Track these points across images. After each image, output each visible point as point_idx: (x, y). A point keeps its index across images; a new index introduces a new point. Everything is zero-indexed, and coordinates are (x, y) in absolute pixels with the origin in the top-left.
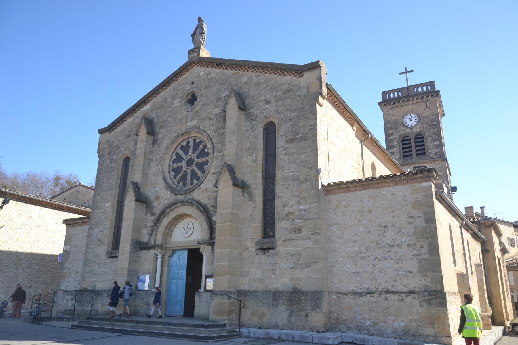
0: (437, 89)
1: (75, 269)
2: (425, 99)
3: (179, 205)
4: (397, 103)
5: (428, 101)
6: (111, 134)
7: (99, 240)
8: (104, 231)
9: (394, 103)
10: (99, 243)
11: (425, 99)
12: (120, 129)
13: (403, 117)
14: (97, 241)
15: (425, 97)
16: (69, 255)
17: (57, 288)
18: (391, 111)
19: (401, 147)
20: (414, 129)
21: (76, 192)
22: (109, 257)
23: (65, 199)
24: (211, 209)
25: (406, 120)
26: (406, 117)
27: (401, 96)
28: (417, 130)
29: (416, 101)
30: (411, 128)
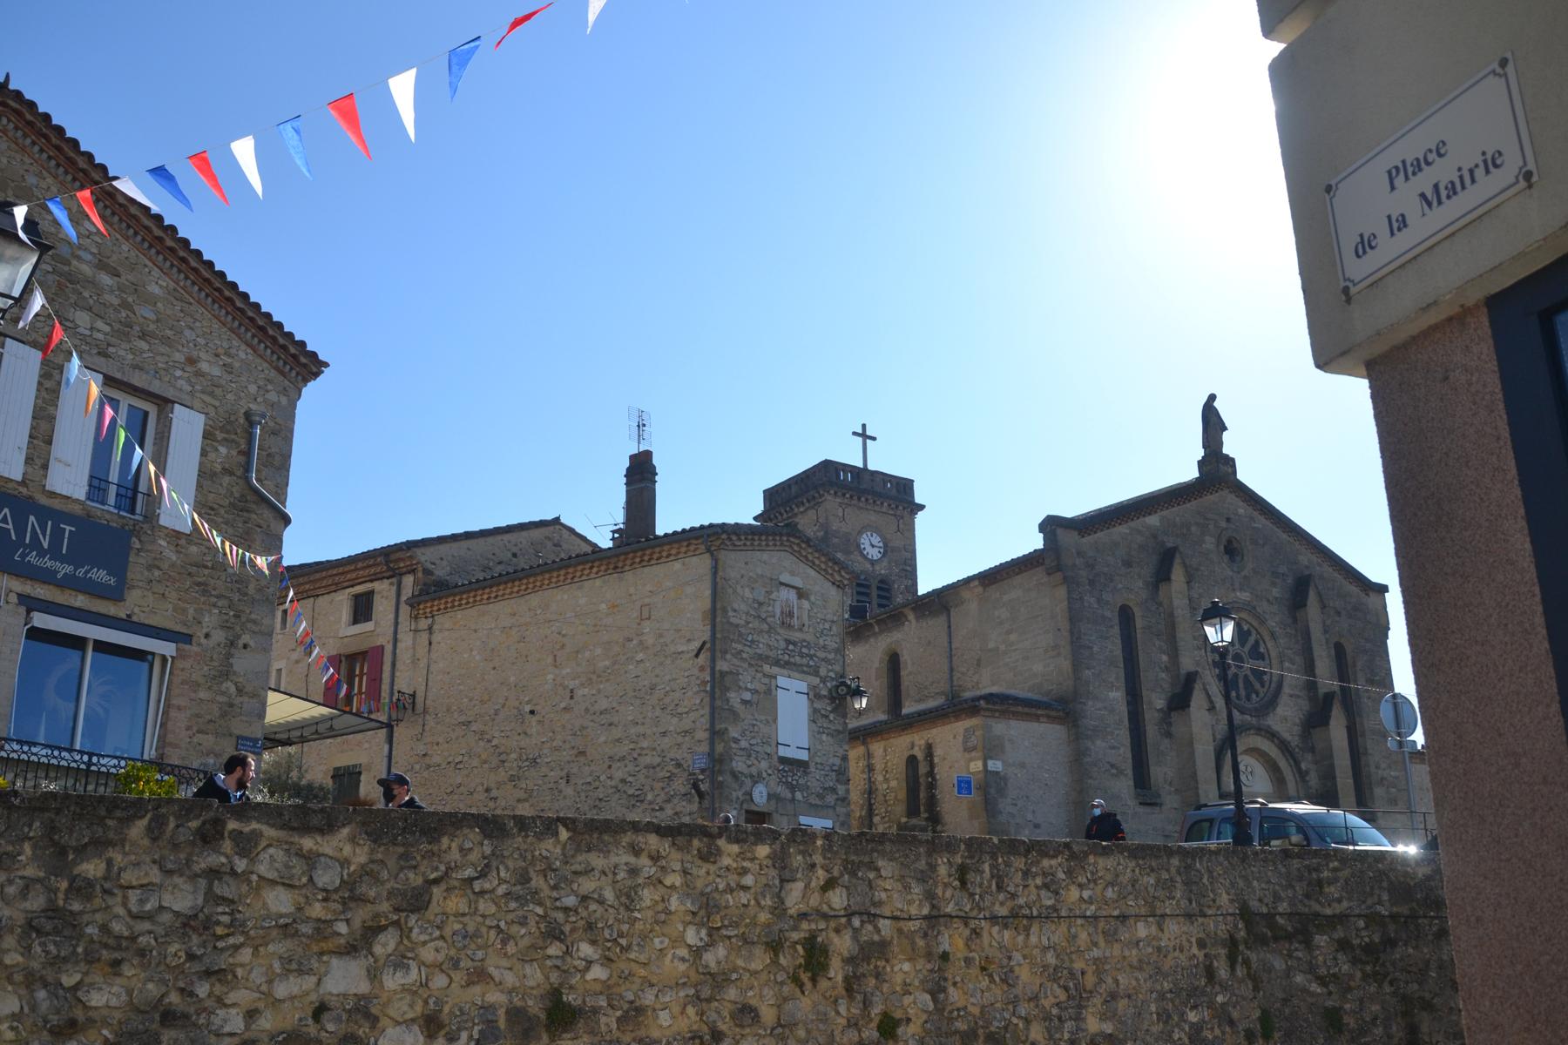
0: (1037, 542)
1: (1030, 817)
2: (898, 513)
3: (1252, 732)
4: (855, 498)
5: (902, 518)
6: (1084, 540)
7: (1112, 766)
8: (1119, 748)
9: (851, 497)
10: (1114, 771)
11: (898, 513)
12: (1101, 536)
13: (860, 533)
14: (1108, 767)
15: (901, 508)
16: (1006, 784)
17: (118, 858)
18: (841, 510)
19: (855, 598)
20: (877, 568)
21: (549, 544)
22: (1141, 804)
23: (515, 555)
24: (1297, 750)
25: (865, 541)
26: (864, 536)
27: (852, 482)
28: (882, 570)
29: (884, 510)
30: (873, 563)
